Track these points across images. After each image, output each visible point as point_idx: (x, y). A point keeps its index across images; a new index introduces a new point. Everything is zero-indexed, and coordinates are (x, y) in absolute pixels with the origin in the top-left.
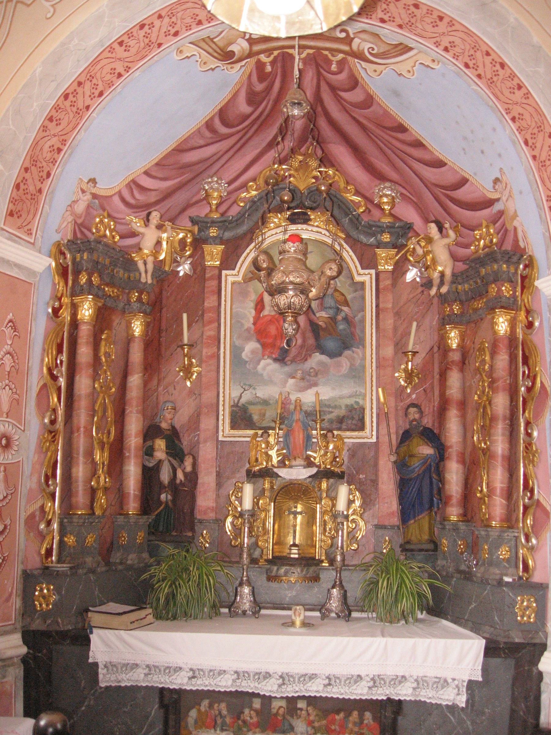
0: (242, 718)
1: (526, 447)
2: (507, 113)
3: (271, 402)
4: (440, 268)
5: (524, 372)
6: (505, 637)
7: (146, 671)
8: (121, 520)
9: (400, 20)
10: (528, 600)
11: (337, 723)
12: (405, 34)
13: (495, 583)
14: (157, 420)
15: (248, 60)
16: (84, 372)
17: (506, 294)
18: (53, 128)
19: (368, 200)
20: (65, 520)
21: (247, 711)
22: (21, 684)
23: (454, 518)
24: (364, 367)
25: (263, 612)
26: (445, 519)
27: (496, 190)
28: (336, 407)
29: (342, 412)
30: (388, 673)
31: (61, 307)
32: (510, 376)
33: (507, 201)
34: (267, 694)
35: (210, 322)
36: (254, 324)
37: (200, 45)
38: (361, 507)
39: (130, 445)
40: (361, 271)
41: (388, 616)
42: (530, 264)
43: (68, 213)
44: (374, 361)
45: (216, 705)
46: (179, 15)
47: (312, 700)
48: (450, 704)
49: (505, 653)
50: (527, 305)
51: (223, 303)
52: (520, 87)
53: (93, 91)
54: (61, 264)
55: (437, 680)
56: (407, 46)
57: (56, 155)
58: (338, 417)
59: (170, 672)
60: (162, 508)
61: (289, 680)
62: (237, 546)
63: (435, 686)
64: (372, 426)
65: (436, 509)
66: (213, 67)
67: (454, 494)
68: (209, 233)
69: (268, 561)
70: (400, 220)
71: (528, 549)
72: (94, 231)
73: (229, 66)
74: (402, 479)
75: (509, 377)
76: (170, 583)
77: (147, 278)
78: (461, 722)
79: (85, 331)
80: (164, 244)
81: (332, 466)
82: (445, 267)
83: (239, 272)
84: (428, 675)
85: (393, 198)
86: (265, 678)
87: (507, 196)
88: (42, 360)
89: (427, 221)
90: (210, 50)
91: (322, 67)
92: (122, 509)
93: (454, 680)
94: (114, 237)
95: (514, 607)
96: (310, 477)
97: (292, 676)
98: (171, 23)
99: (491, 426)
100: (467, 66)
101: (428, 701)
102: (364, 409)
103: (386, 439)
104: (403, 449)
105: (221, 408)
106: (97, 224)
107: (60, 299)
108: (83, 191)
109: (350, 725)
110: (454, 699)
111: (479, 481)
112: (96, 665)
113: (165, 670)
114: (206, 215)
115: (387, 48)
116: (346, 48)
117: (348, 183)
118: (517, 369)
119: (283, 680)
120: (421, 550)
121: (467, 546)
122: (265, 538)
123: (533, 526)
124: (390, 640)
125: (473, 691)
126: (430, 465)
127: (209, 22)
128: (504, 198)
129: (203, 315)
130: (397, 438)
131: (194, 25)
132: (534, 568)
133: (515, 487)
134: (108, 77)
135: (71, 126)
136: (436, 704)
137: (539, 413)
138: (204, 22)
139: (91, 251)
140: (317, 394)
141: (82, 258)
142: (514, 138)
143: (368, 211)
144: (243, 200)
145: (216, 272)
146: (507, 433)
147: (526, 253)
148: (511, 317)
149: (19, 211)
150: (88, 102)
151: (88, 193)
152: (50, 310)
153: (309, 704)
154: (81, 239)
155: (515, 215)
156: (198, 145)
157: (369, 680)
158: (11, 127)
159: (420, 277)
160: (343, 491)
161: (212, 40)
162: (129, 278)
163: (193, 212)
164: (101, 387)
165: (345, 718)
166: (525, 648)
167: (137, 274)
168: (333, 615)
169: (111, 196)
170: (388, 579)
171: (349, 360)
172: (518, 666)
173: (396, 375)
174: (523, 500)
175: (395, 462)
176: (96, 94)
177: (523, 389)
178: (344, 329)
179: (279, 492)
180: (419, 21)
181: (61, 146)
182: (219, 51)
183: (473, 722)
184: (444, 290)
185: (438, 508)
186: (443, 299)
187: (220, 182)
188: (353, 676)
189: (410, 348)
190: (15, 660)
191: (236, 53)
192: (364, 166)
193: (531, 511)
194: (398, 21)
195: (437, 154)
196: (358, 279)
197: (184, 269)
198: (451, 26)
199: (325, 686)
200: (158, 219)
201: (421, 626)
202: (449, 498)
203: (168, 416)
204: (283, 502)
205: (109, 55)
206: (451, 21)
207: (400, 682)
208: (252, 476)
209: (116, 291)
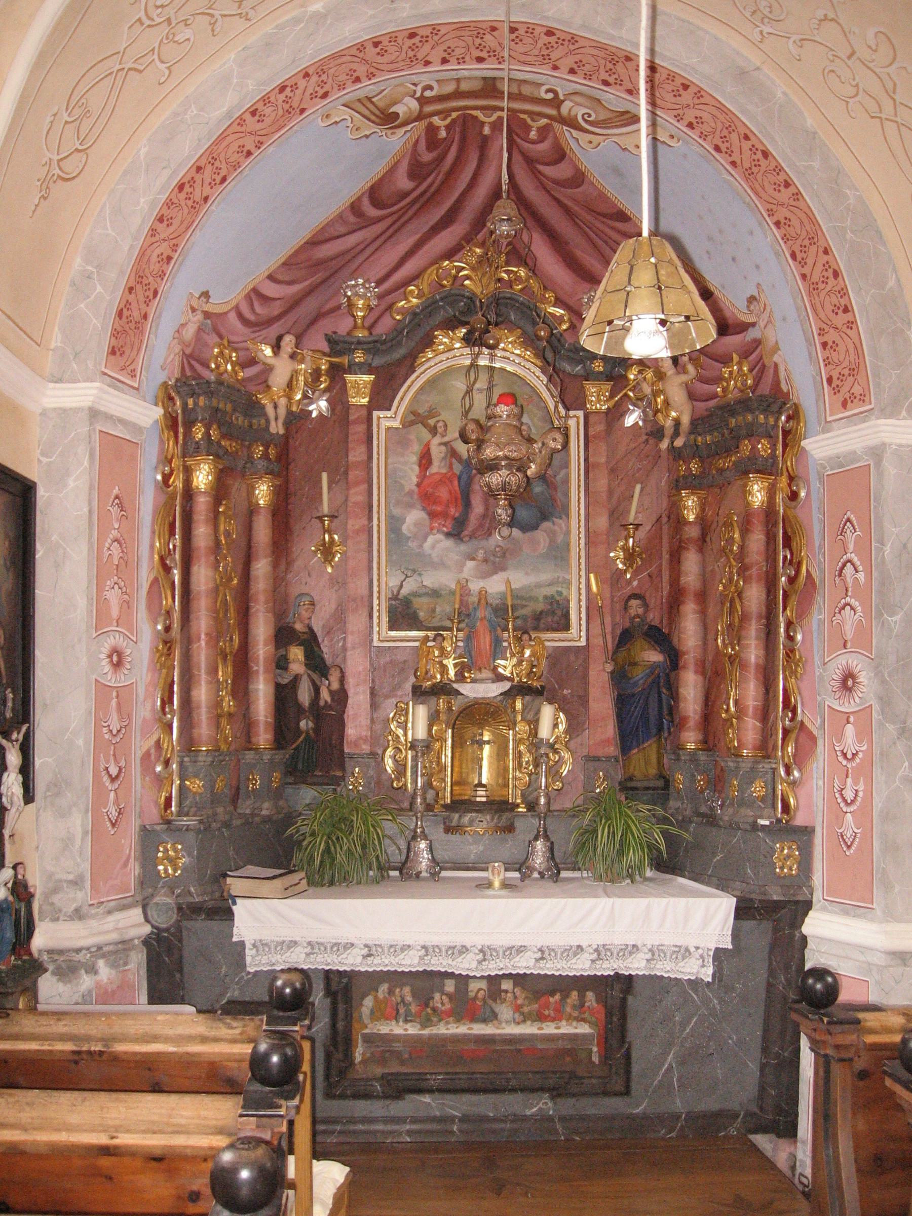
0: (431, 1005)
1: (787, 653)
2: (769, 215)
3: (443, 593)
4: (674, 414)
5: (785, 557)
6: (761, 894)
7: (308, 950)
8: (250, 756)
9: (629, 84)
10: (790, 848)
11: (552, 1007)
13: (749, 828)
14: (290, 619)
16: (203, 560)
18: (164, 231)
20: (186, 759)
21: (437, 996)
22: (144, 972)
23: (691, 746)
24: (568, 545)
25: (444, 874)
26: (679, 747)
27: (751, 312)
28: (531, 599)
29: (540, 606)
30: (616, 942)
31: (172, 471)
32: (767, 561)
33: (765, 327)
34: (464, 973)
35: (357, 483)
36: (418, 485)
37: (353, 106)
38: (566, 732)
39: (258, 656)
41: (609, 873)
42: (795, 415)
43: (176, 340)
44: (582, 536)
45: (398, 990)
46: (332, 71)
47: (519, 979)
48: (693, 978)
49: (761, 914)
50: (790, 469)
51: (375, 456)
52: (787, 185)
55: (677, 949)
58: (534, 611)
59: (338, 950)
60: (301, 739)
61: (491, 955)
62: (400, 788)
63: (674, 956)
64: (580, 625)
65: (666, 734)
66: (368, 133)
67: (692, 715)
69: (446, 807)
71: (789, 784)
72: (213, 366)
74: (619, 695)
75: (764, 563)
76: (325, 838)
78: (706, 1001)
79: (202, 504)
81: (529, 679)
82: (681, 412)
83: (396, 413)
84: (666, 943)
86: (461, 953)
88: (152, 546)
90: (367, 113)
91: (517, 135)
92: (250, 742)
93: (697, 948)
95: (772, 857)
96: (501, 694)
97: (495, 950)
98: (319, 83)
99: (741, 628)
100: (717, 149)
101: (666, 975)
102: (568, 601)
103: (600, 641)
104: (622, 654)
105: (376, 602)
106: (217, 357)
107: (170, 462)
108: (194, 310)
109: (568, 1009)
110: (698, 973)
111: (724, 696)
112: (242, 944)
113: (332, 948)
114: (349, 334)
115: (609, 115)
116: (553, 112)
117: (545, 288)
118: (775, 552)
119: (484, 955)
120: (648, 788)
121: (708, 782)
122: (442, 776)
123: (794, 756)
124: (618, 901)
125: (720, 963)
126: (659, 677)
127: (370, 79)
128: (762, 324)
129: (346, 473)
130: (613, 642)
131: (349, 83)
132: (797, 808)
133: (772, 704)
134: (236, 157)
135: (185, 225)
136: (676, 978)
137: (803, 612)
138: (363, 78)
139: (210, 394)
140: (508, 582)
142: (778, 248)
144: (401, 311)
145: (364, 412)
146: (763, 635)
147: (790, 400)
148: (769, 484)
150: (207, 191)
151: (199, 312)
152: (159, 477)
153: (515, 985)
155: (776, 349)
156: (336, 234)
157: (592, 951)
158: (110, 232)
159: (644, 421)
160: (547, 712)
161: (369, 99)
162: (251, 426)
163: (327, 325)
164: (222, 578)
165: (561, 1000)
166: (784, 908)
167: (263, 421)
168: (536, 875)
169: (226, 313)
170: (609, 827)
171: (548, 535)
172: (776, 930)
173: (612, 554)
174: (782, 721)
175: (612, 673)
176: (218, 180)
177: (783, 579)
178: (542, 493)
179: (459, 715)
181: (171, 254)
182: (377, 112)
183: (721, 1001)
184: (679, 442)
185: (670, 733)
186: (676, 454)
188: (571, 947)
189: (631, 518)
190: (136, 942)
192: (565, 261)
193: (793, 736)
198: (698, 98)
199: (537, 960)
201: (651, 884)
202: (684, 721)
203: (305, 614)
204: (465, 728)
205: (239, 129)
206: (699, 92)
207: (631, 953)
208: (419, 693)
209: (234, 444)
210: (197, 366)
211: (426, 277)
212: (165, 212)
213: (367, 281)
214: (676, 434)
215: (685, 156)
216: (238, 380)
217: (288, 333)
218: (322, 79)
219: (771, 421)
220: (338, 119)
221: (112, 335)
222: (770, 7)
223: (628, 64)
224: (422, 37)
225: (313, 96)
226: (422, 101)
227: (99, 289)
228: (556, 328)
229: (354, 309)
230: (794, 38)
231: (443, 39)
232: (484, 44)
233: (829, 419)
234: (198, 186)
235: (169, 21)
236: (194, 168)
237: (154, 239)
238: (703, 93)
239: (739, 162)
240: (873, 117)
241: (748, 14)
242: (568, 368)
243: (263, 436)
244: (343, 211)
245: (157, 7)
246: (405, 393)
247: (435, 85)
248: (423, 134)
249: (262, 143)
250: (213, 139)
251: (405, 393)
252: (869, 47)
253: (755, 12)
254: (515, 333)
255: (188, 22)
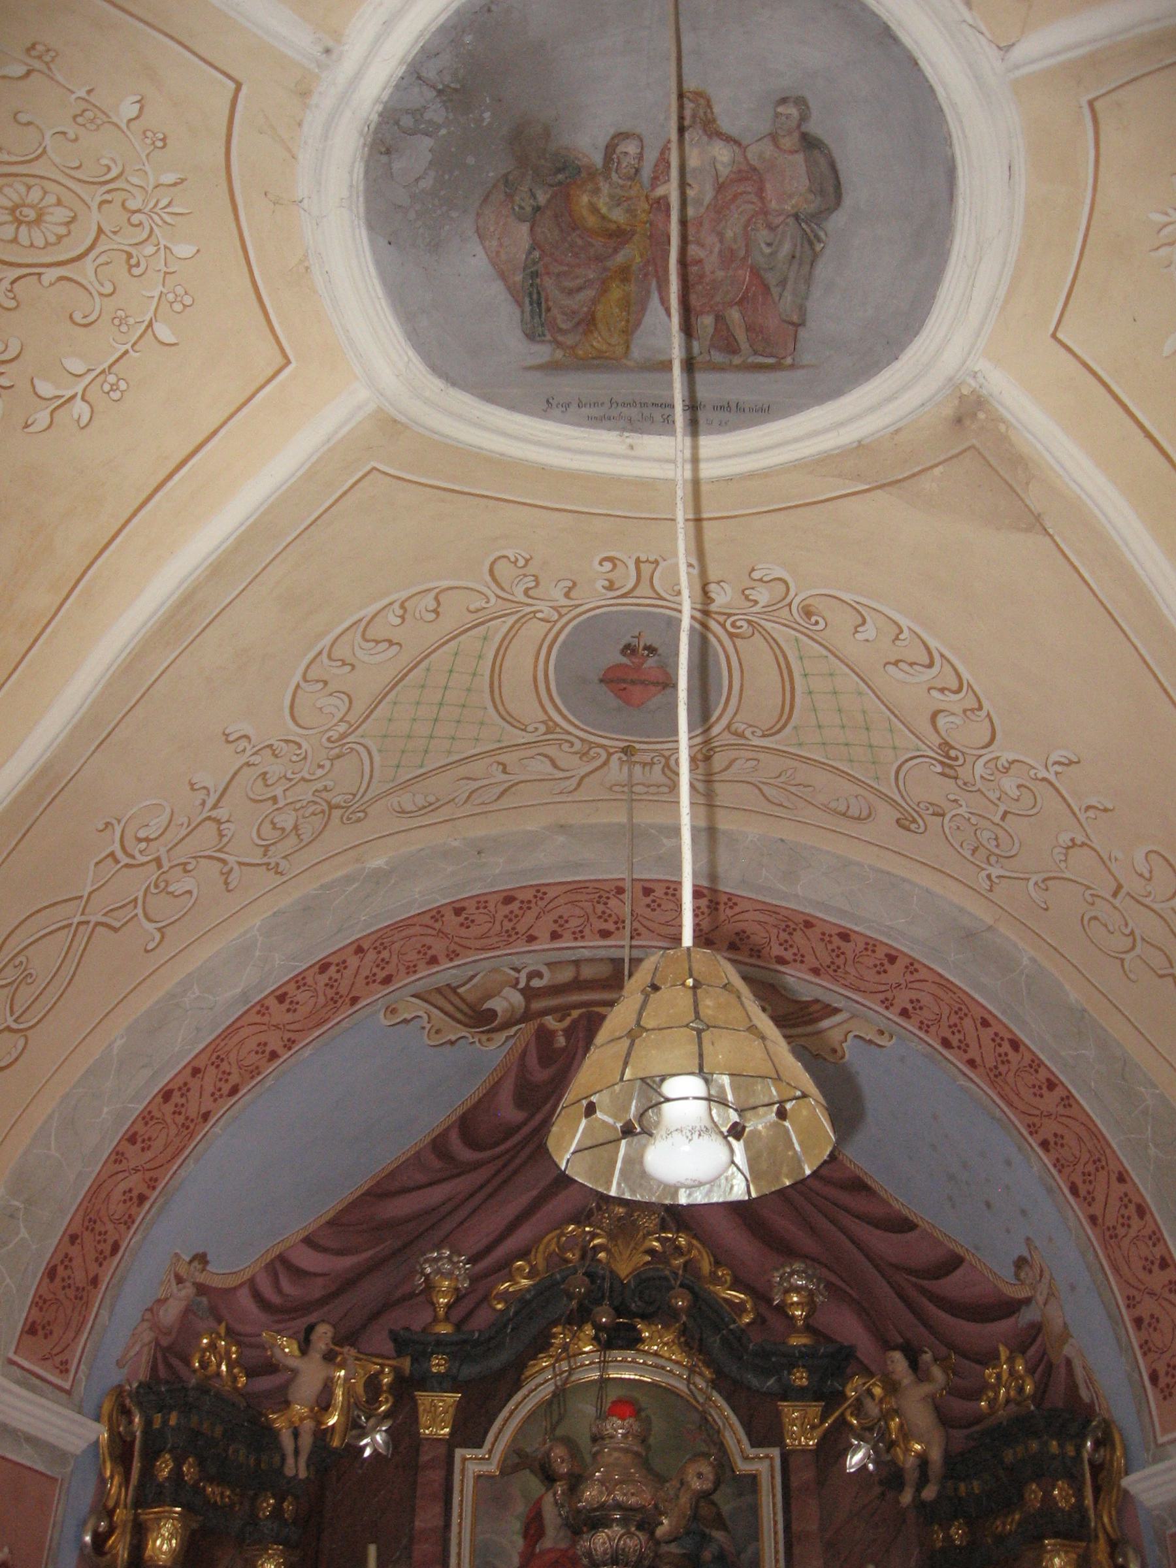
2: (1031, 1133)
9: (814, 960)
12: (825, 984)
15: (523, 1025)
17: (1062, 1504)
19: (761, 1296)
31: (111, 1530)
33: (1045, 1304)
40: (752, 1452)
46: (396, 946)
51: (455, 1520)
52: (1051, 1085)
53: (219, 1085)
54: (119, 1433)
56: (828, 1006)
57: (134, 1210)
66: (453, 1038)
68: (431, 1366)
70: (829, 1339)
73: (484, 1038)
77: (297, 1468)
80: (339, 1393)
83: (490, 1452)
85: (811, 1293)
87: (1045, 1292)
89: (888, 1346)
94: (235, 1379)
98: (379, 961)
100: (946, 1043)
106: (204, 1350)
107: (110, 1513)
108: (180, 1280)
114: (424, 1330)
117: (717, 1263)
127: (451, 960)
128: (1040, 1299)
131: (421, 965)
134: (254, 1058)
135: (171, 1150)
138: (442, 957)
141: (165, 1422)
142: (1051, 1181)
143: (760, 1320)
144: (504, 1296)
145: (442, 1450)
148: (1079, 1556)
149: (49, 1324)
151: (188, 1284)
152: (88, 1539)
154: (167, 1382)
155: (1065, 1336)
159: (876, 1463)
161: (454, 990)
163: (396, 1319)
167: (277, 1459)
169: (235, 1289)
176: (226, 1090)
180: (850, 962)
181: (146, 1192)
186: (928, 1513)
187: (455, 1259)
191: (500, 1014)
194: (811, 961)
195: (897, 1206)
196: (742, 1467)
197: (374, 1442)
200: (329, 1341)
205: (258, 1019)
206: (912, 964)
209: (228, 1493)
210: (175, 1362)
211: (541, 1248)
212: (140, 1128)
213: (456, 1252)
214: (923, 1479)
215: (902, 1059)
216: (236, 1389)
217: (323, 1321)
218: (381, 956)
219: (1070, 1450)
220: (408, 1016)
221: (34, 1303)
222: (996, 839)
223: (809, 932)
224: (522, 902)
225: (370, 980)
226: (529, 993)
227: (24, 1233)
228: (734, 1322)
229: (434, 1294)
230: (1034, 878)
231: (552, 905)
232: (608, 911)
233: (1161, 1440)
234: (194, 1094)
235: (158, 861)
236: (189, 1070)
237: (119, 1167)
238: (916, 965)
239: (978, 1060)
240: (1161, 976)
241: (968, 854)
242: (755, 1382)
243: (282, 1488)
244: (421, 1150)
245: (140, 840)
246: (506, 1421)
247: (544, 970)
248: (534, 1038)
249: (294, 1042)
250: (219, 1031)
251: (506, 1421)
252: (1141, 875)
253: (974, 851)
254: (672, 1330)
255: (189, 867)
